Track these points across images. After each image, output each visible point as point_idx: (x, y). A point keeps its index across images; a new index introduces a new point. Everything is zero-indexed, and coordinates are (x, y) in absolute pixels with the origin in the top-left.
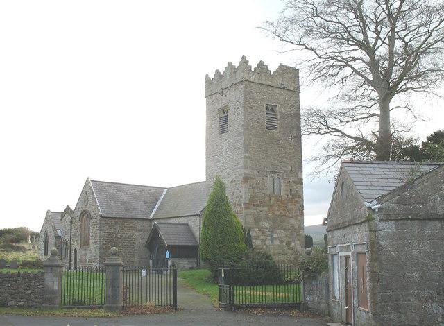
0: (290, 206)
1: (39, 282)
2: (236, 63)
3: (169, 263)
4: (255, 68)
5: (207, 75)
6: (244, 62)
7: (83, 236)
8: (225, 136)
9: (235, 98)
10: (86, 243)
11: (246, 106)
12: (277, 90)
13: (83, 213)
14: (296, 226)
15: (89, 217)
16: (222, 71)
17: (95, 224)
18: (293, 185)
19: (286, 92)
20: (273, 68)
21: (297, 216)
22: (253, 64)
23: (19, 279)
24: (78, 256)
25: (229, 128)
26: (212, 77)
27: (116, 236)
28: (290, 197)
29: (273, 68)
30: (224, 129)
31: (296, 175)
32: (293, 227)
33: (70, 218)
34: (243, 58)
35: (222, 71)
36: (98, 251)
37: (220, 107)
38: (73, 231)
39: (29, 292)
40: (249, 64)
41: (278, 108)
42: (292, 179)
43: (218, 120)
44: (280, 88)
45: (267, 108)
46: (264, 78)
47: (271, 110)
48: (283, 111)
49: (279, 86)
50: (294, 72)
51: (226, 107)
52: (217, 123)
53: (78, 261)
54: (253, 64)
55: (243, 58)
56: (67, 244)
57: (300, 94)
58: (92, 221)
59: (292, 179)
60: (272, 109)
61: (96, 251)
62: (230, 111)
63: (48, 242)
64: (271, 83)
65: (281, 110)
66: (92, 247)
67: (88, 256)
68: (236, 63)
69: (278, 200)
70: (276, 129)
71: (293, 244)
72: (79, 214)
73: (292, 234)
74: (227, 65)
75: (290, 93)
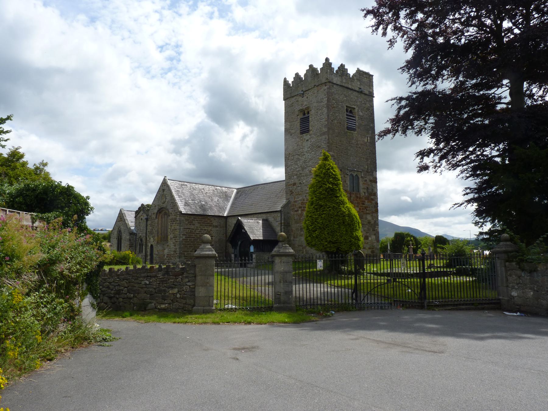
0: (367, 203)
1: (186, 277)
2: (319, 66)
3: (254, 256)
4: (337, 71)
5: (285, 79)
6: (327, 64)
7: (160, 233)
8: (306, 136)
9: (316, 100)
10: (163, 239)
11: (329, 107)
12: (355, 93)
13: (160, 211)
14: (372, 222)
15: (167, 214)
16: (302, 75)
17: (174, 220)
18: (369, 183)
19: (363, 95)
20: (351, 71)
21: (373, 212)
22: (335, 66)
23: (160, 275)
24: (155, 251)
25: (310, 128)
26: (290, 80)
27: (195, 231)
28: (366, 194)
29: (351, 71)
30: (305, 129)
31: (372, 175)
32: (369, 223)
33: (145, 217)
34: (327, 59)
35: (302, 75)
36: (177, 247)
37: (301, 108)
38: (149, 228)
39: (176, 291)
40: (332, 66)
41: (356, 110)
42: (368, 178)
43: (299, 121)
44: (358, 92)
45: (347, 111)
46: (344, 81)
47: (350, 111)
48: (361, 114)
49: (357, 89)
50: (369, 77)
51: (308, 108)
52: (297, 124)
53: (154, 256)
54: (335, 66)
55: (327, 59)
56: (141, 240)
57: (374, 98)
58: (170, 218)
59: (368, 178)
60: (351, 112)
61: (175, 246)
62: (312, 112)
63: (121, 239)
64: (350, 87)
65: (359, 113)
66: (171, 243)
67: (166, 251)
68: (319, 66)
69: (357, 197)
70: (354, 130)
71: (370, 239)
72: (156, 211)
73: (369, 230)
74: (308, 68)
75: (366, 97)
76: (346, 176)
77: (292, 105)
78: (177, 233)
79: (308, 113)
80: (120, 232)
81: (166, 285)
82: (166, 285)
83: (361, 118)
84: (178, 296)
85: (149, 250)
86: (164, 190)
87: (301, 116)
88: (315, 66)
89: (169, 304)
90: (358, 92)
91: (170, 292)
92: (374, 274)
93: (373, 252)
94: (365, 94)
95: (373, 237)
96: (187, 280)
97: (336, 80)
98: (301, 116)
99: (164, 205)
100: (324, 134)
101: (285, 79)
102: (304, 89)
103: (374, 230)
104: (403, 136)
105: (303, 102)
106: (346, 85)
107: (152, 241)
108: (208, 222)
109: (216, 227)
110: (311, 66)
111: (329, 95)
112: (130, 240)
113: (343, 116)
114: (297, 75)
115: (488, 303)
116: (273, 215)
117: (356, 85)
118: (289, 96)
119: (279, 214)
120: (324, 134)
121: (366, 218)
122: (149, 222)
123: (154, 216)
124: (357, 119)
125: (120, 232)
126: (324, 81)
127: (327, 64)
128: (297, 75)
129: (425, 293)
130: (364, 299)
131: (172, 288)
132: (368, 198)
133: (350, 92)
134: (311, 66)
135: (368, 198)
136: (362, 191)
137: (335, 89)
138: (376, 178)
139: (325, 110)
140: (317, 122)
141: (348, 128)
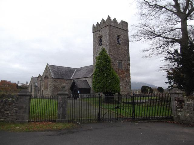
1: (14, 105)
2: (105, 19)
3: (79, 95)
5: (93, 25)
6: (109, 18)
9: (105, 33)
10: (46, 88)
11: (110, 35)
14: (128, 81)
22: (112, 19)
25: (103, 44)
26: (95, 25)
34: (109, 16)
38: (42, 84)
41: (121, 36)
42: (126, 63)
43: (98, 41)
47: (118, 37)
49: (121, 28)
52: (98, 42)
54: (112, 19)
55: (109, 16)
56: (39, 89)
59: (126, 63)
60: (119, 37)
64: (118, 27)
67: (47, 93)
68: (105, 19)
70: (120, 44)
71: (127, 88)
73: (126, 84)
75: (125, 31)
76: (117, 62)
77: (95, 35)
78: (51, 85)
79: (102, 38)
80: (31, 85)
81: (4, 109)
82: (4, 109)
83: (123, 39)
84: (9, 114)
85: (41, 92)
86: (47, 69)
87: (99, 39)
88: (104, 19)
89: (5, 118)
90: (122, 29)
91: (6, 113)
92: (125, 103)
93: (128, 93)
94: (125, 30)
95: (128, 87)
96: (14, 107)
97: (112, 24)
98: (99, 39)
99: (47, 75)
100: (107, 46)
101: (93, 25)
102: (100, 28)
103: (128, 84)
104: (175, 49)
105: (100, 33)
106: (117, 26)
107: (42, 89)
108: (64, 81)
109: (67, 83)
110: (103, 19)
111: (110, 30)
112: (35, 89)
113: (115, 38)
114: (98, 23)
115: (45, 131)
116: (88, 78)
117: (121, 27)
118: (94, 31)
119: (90, 78)
120: (107, 46)
121: (125, 80)
122: (42, 82)
123: (43, 79)
124: (121, 40)
125: (31, 85)
126: (107, 25)
127: (109, 18)
128: (98, 23)
129: (134, 114)
130: (103, 117)
131: (7, 111)
132: (126, 71)
133: (119, 29)
134: (103, 19)
135: (126, 71)
136: (123, 68)
137: (112, 28)
138: (129, 64)
139: (108, 36)
140: (105, 41)
141: (118, 44)
